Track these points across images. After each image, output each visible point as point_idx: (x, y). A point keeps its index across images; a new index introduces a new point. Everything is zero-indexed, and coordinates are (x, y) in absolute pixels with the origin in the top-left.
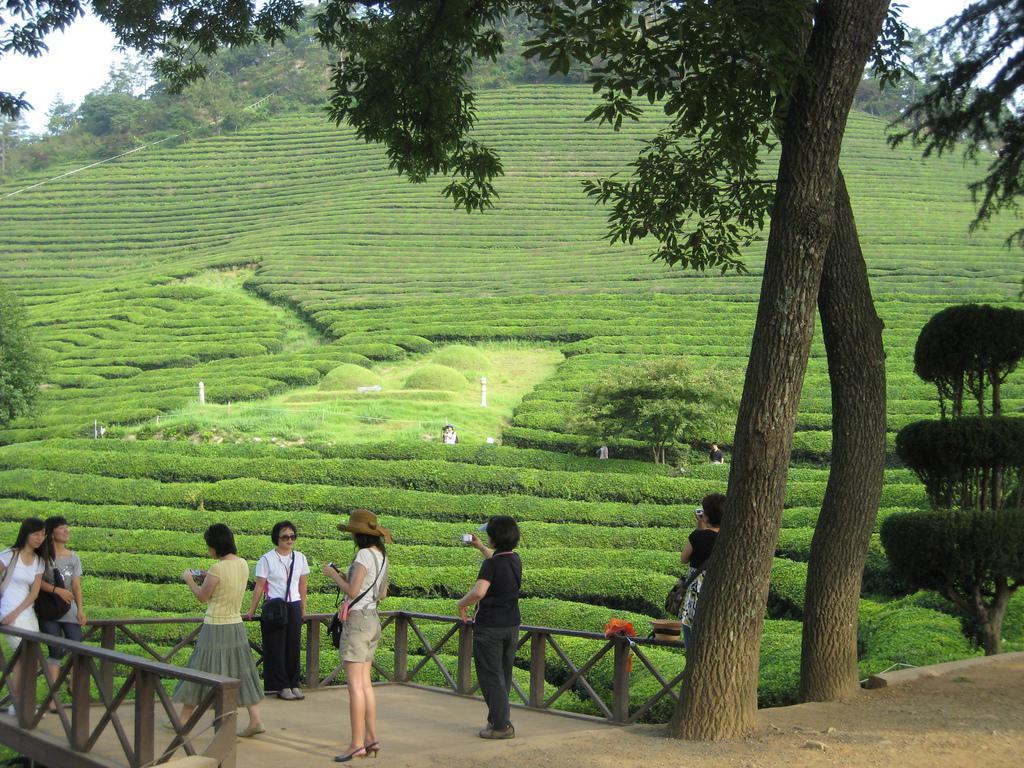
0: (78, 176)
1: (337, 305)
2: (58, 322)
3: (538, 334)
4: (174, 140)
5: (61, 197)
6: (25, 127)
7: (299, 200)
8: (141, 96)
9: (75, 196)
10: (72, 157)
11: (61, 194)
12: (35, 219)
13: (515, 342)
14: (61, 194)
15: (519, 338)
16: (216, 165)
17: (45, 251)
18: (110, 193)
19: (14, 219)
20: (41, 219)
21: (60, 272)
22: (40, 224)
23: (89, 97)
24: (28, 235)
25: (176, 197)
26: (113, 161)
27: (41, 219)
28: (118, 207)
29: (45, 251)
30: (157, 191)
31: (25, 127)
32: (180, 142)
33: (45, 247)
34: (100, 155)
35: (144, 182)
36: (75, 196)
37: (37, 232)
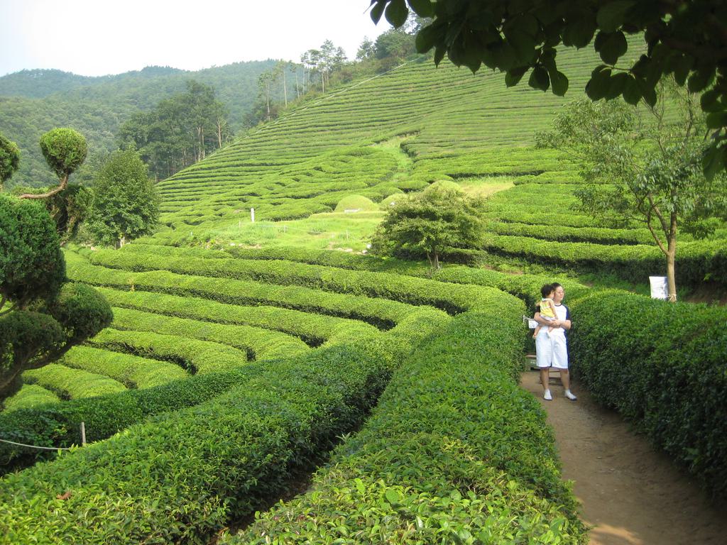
0: (366, 84)
1: (440, 155)
2: (432, 159)
3: (518, 171)
4: (422, 58)
5: (353, 98)
6: (345, 58)
7: (475, 90)
8: (410, 33)
9: (360, 97)
10: (365, 73)
11: (352, 96)
12: (335, 112)
13: (504, 177)
14: (352, 96)
15: (507, 174)
16: (442, 72)
17: (332, 130)
18: (378, 93)
19: (325, 112)
20: (337, 111)
21: (334, 142)
22: (336, 114)
23: (71, 73)
24: (327, 121)
25: (414, 93)
26: (386, 74)
27: (337, 111)
28: (379, 101)
29: (332, 130)
30: (403, 90)
31: (345, 58)
32: (426, 59)
33: (332, 128)
34: (380, 71)
35: (399, 85)
36: (360, 97)
37: (331, 119)
